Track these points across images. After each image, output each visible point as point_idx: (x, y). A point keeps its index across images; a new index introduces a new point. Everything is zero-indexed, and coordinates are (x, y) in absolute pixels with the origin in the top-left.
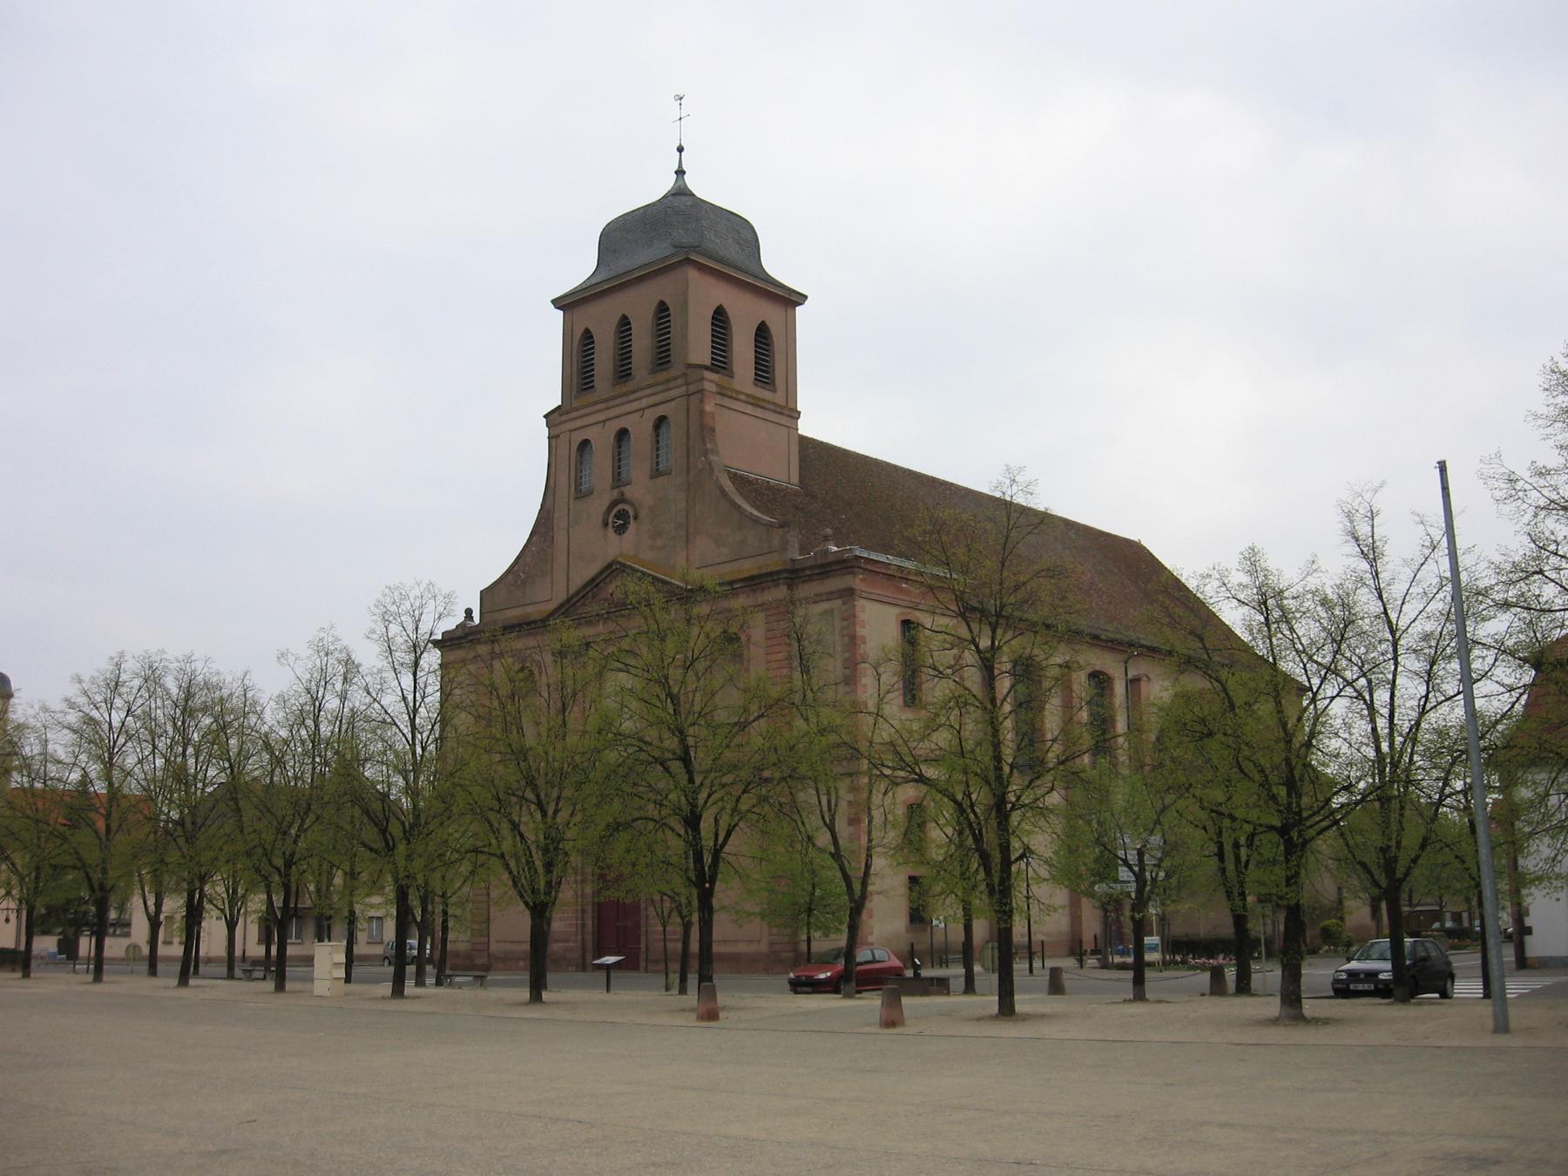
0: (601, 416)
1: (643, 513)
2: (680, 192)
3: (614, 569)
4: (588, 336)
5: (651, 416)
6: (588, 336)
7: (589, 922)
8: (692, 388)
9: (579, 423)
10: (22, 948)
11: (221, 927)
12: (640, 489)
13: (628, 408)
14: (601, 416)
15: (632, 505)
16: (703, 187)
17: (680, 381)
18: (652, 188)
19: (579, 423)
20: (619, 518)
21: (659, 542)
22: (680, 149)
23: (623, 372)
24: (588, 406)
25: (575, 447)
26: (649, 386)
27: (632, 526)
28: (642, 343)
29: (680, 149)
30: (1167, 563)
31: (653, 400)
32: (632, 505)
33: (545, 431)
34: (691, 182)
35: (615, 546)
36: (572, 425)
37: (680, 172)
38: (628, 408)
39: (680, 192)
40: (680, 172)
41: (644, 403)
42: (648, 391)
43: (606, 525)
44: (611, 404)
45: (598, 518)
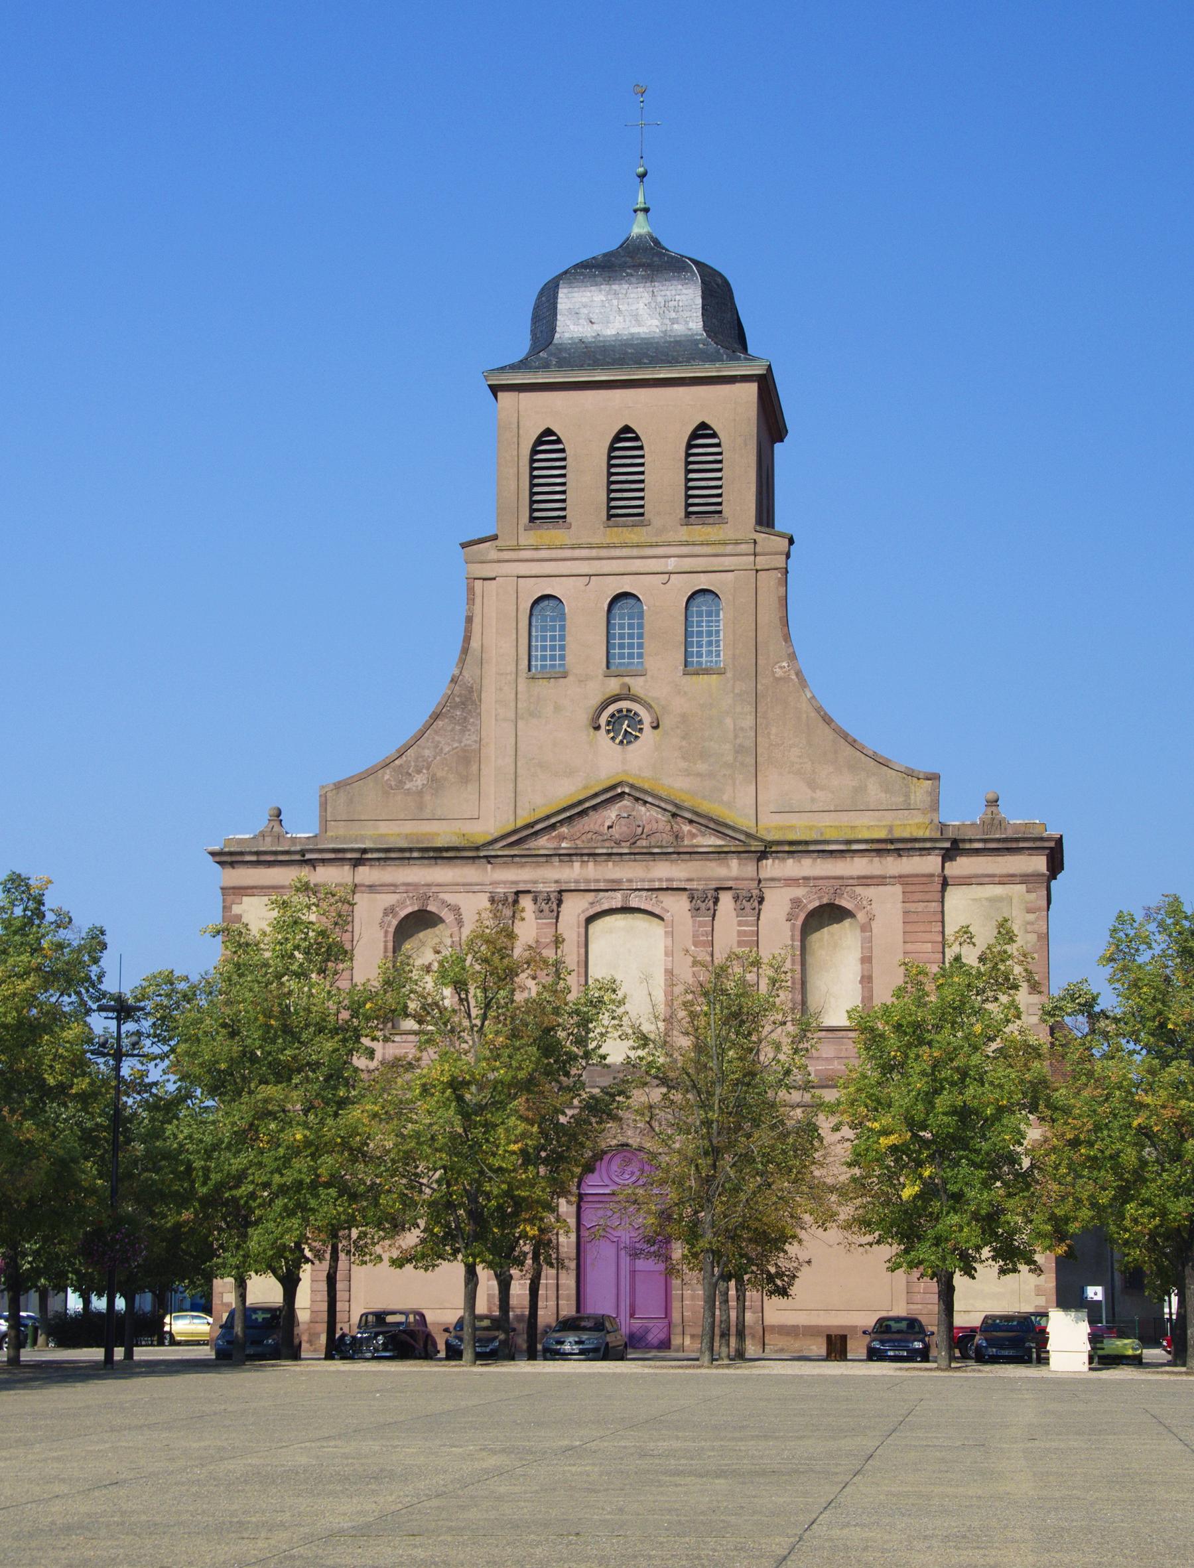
1: (666, 723)
3: (612, 794)
5: (685, 586)
9: (536, 568)
13: (716, 563)
15: (648, 706)
17: (744, 548)
31: (688, 564)
35: (609, 761)
38: (716, 563)
41: (672, 564)
45: (583, 717)
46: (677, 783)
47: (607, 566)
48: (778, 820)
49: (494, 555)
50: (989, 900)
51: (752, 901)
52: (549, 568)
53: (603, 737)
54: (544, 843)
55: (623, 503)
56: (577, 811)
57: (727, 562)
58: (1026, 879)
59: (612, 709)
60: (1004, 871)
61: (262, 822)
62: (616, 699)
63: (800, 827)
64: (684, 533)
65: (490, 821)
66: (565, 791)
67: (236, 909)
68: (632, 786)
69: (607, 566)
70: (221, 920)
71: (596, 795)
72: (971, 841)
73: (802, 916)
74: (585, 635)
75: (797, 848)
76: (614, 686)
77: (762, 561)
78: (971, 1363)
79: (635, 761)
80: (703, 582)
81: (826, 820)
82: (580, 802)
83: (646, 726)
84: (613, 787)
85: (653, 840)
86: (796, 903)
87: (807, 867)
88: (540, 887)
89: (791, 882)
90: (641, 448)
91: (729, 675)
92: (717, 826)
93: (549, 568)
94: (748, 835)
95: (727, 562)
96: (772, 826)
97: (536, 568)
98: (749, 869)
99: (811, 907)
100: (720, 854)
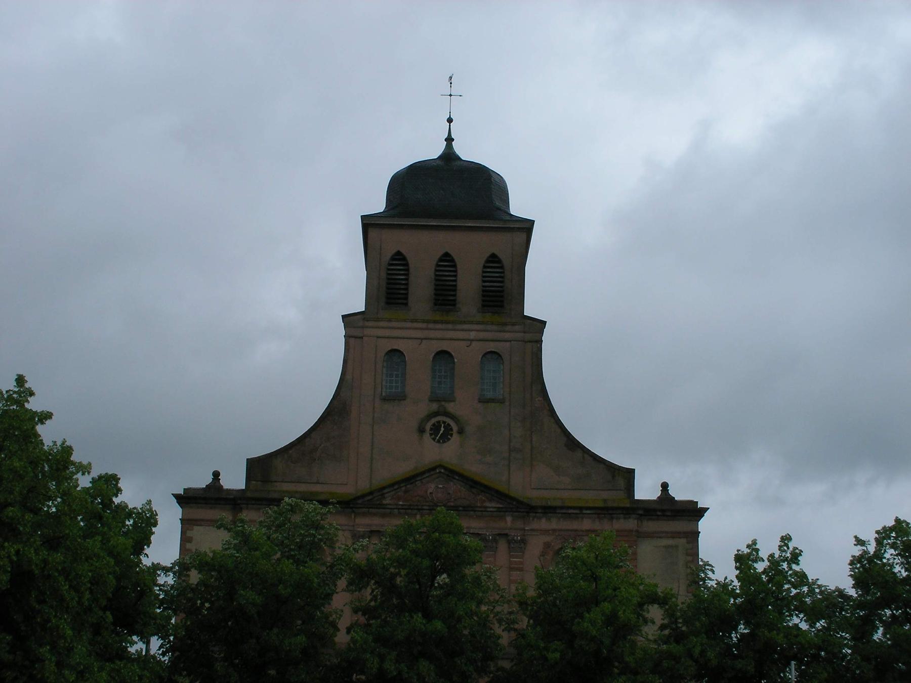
0: (419, 334)
2: (449, 156)
8: (528, 336)
9: (387, 333)
12: (464, 405)
14: (419, 334)
16: (466, 152)
18: (433, 151)
19: (387, 333)
22: (450, 120)
23: (445, 296)
26: (478, 323)
27: (455, 438)
28: (469, 283)
29: (450, 120)
30: (364, 274)
31: (482, 335)
32: (453, 417)
33: (341, 331)
34: (458, 148)
35: (431, 452)
36: (380, 332)
37: (449, 140)
39: (449, 156)
40: (449, 140)
41: (473, 335)
43: (421, 431)
46: (474, 468)
47: (432, 334)
51: (518, 545)
61: (209, 479)
62: (436, 414)
66: (404, 468)
67: (189, 534)
69: (432, 334)
74: (419, 379)
75: (548, 510)
76: (434, 407)
79: (449, 452)
80: (492, 347)
86: (547, 545)
87: (554, 524)
89: (546, 532)
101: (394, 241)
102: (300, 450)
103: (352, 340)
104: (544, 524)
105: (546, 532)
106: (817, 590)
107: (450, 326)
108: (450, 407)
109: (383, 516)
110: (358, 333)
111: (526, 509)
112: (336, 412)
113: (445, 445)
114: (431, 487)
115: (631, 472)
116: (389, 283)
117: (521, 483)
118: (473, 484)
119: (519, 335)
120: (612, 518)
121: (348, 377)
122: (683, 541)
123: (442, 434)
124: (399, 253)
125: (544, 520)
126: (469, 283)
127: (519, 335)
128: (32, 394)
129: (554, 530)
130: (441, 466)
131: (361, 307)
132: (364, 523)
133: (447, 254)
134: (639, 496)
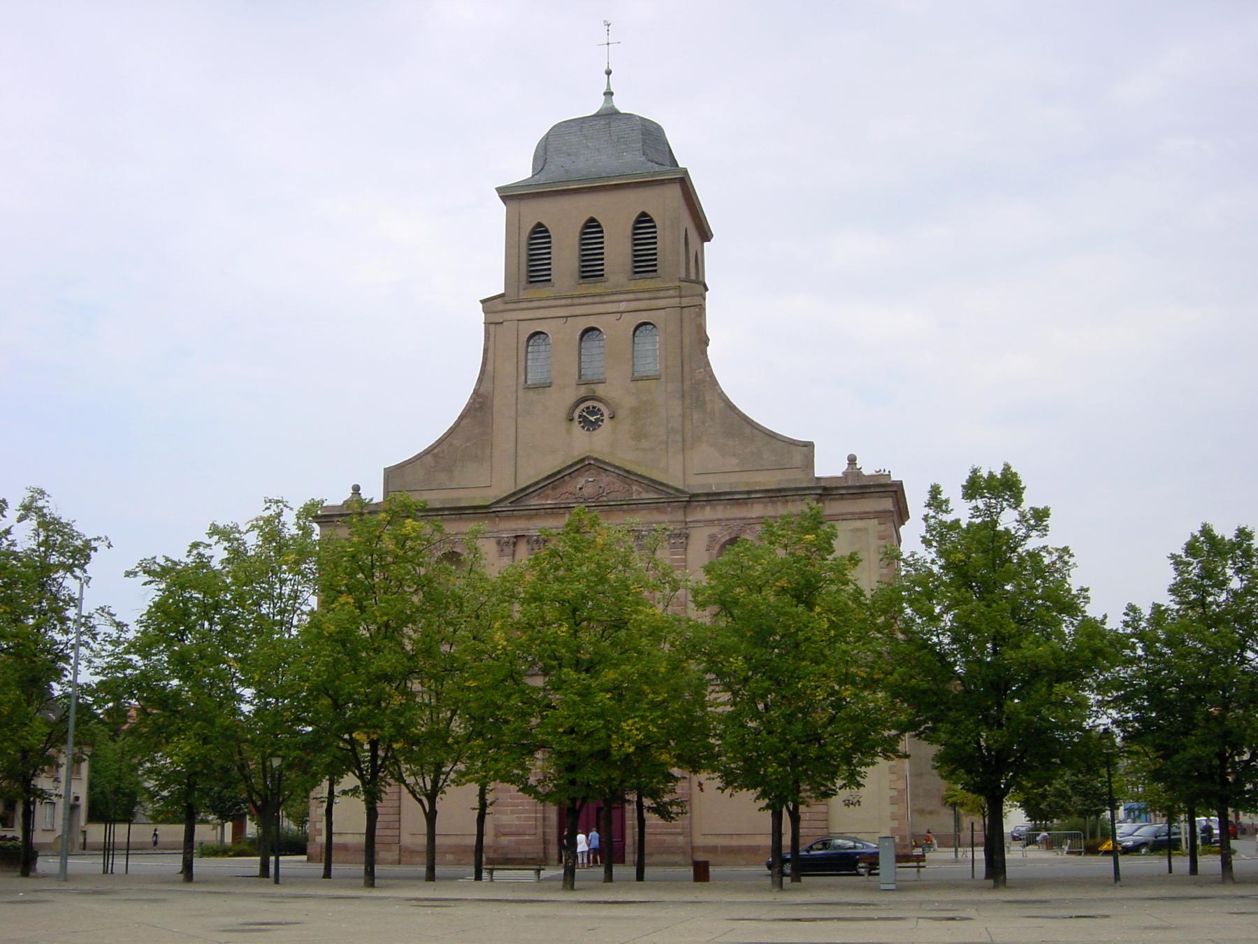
1: (621, 414)
3: (585, 465)
4: (540, 231)
5: (632, 320)
6: (540, 231)
7: (1070, 896)
9: (530, 314)
10: (272, 858)
11: (358, 806)
13: (654, 304)
15: (606, 404)
16: (622, 104)
17: (672, 292)
18: (593, 106)
20: (588, 413)
21: (644, 444)
22: (609, 73)
23: (591, 268)
24: (540, 300)
25: (524, 338)
28: (617, 249)
29: (609, 73)
31: (634, 305)
32: (606, 404)
33: (481, 317)
35: (582, 443)
37: (609, 94)
38: (654, 304)
40: (609, 94)
41: (623, 306)
42: (631, 296)
44: (576, 301)
45: (562, 413)
46: (626, 457)
47: (578, 310)
48: (701, 480)
49: (501, 307)
50: (852, 530)
51: (682, 538)
52: (539, 313)
53: (576, 426)
54: (534, 502)
55: (591, 268)
56: (556, 479)
57: (661, 303)
58: (880, 515)
59: (583, 406)
60: (880, 509)
61: (348, 494)
63: (715, 483)
64: (632, 286)
65: (503, 486)
66: (551, 464)
68: (596, 459)
69: (578, 310)
70: (1174, 574)
71: (570, 466)
72: (837, 488)
73: (717, 547)
75: (712, 498)
76: (583, 391)
77: (685, 301)
78: (152, 838)
79: (598, 443)
80: (644, 317)
81: (734, 478)
82: (559, 472)
83: (606, 417)
84: (582, 460)
85: (611, 497)
86: (713, 538)
87: (720, 512)
88: (532, 533)
89: (711, 522)
90: (654, 227)
91: (663, 379)
92: (654, 484)
93: (539, 313)
94: (677, 490)
95: (661, 303)
96: (697, 484)
97: (530, 314)
98: (679, 516)
99: (723, 540)
100: (654, 506)
101: (535, 212)
102: (440, 456)
103: (492, 327)
104: (708, 513)
105: (711, 522)
106: (278, 618)
107: (597, 299)
108: (600, 390)
109: (530, 517)
110: (498, 318)
111: (691, 500)
112: (479, 407)
113: (595, 432)
114: (581, 481)
115: (809, 446)
116: (532, 256)
117: (674, 471)
118: (627, 475)
119: (675, 301)
120: (787, 501)
121: (489, 368)
122: (875, 521)
123: (590, 422)
124: (540, 225)
125: (708, 509)
126: (617, 249)
127: (675, 301)
128: (1206, 531)
129: (719, 520)
130: (588, 458)
131: (501, 290)
132: (508, 528)
133: (592, 220)
134: (818, 473)
